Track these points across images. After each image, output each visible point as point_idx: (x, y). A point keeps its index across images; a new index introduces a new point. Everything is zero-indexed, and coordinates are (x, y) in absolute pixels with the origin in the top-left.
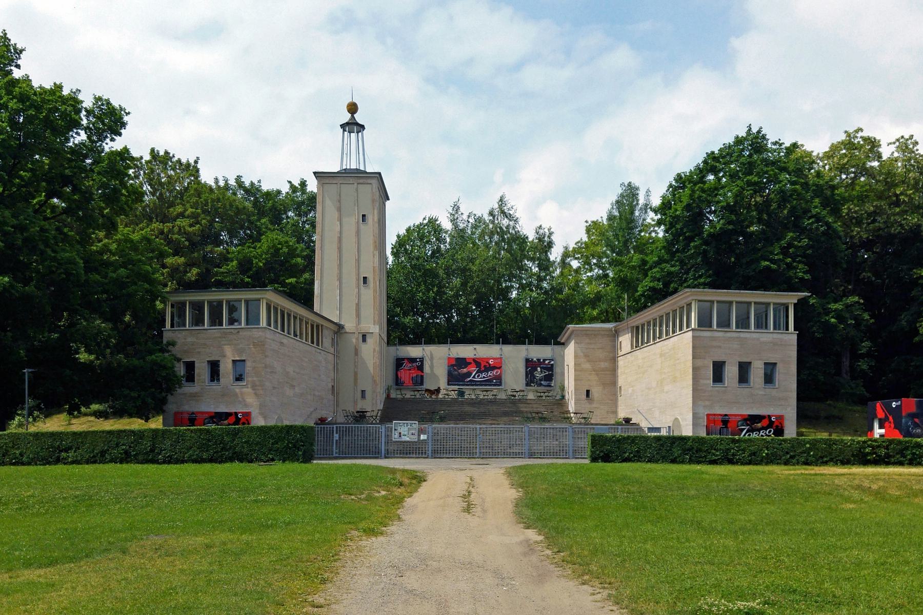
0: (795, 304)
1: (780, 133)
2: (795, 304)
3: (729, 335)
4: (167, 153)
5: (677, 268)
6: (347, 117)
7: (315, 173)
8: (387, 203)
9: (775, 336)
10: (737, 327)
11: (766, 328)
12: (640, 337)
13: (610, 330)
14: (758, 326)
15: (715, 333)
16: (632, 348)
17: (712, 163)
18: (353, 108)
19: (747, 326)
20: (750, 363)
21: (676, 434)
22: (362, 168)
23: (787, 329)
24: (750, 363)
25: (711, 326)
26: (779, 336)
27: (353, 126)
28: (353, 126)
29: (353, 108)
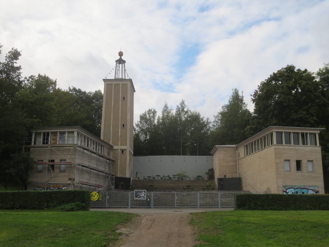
0: (319, 133)
1: (300, 65)
2: (319, 133)
3: (291, 147)
4: (48, 77)
5: (57, 241)
6: (118, 57)
7: (104, 80)
8: (135, 93)
9: (311, 148)
10: (285, 144)
11: (290, 144)
12: (250, 150)
13: (234, 147)
14: (303, 144)
15: (284, 147)
16: (245, 155)
17: (275, 77)
18: (121, 54)
19: (298, 144)
20: (301, 160)
21: (268, 193)
22: (124, 78)
23: (316, 145)
24: (301, 160)
25: (282, 144)
26: (313, 148)
27: (120, 61)
28: (120, 61)
29: (121, 54)
